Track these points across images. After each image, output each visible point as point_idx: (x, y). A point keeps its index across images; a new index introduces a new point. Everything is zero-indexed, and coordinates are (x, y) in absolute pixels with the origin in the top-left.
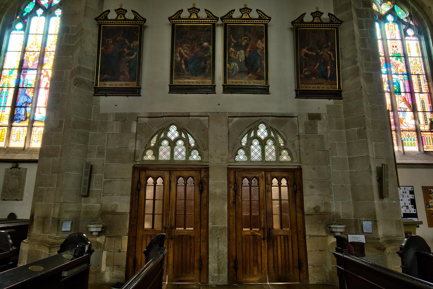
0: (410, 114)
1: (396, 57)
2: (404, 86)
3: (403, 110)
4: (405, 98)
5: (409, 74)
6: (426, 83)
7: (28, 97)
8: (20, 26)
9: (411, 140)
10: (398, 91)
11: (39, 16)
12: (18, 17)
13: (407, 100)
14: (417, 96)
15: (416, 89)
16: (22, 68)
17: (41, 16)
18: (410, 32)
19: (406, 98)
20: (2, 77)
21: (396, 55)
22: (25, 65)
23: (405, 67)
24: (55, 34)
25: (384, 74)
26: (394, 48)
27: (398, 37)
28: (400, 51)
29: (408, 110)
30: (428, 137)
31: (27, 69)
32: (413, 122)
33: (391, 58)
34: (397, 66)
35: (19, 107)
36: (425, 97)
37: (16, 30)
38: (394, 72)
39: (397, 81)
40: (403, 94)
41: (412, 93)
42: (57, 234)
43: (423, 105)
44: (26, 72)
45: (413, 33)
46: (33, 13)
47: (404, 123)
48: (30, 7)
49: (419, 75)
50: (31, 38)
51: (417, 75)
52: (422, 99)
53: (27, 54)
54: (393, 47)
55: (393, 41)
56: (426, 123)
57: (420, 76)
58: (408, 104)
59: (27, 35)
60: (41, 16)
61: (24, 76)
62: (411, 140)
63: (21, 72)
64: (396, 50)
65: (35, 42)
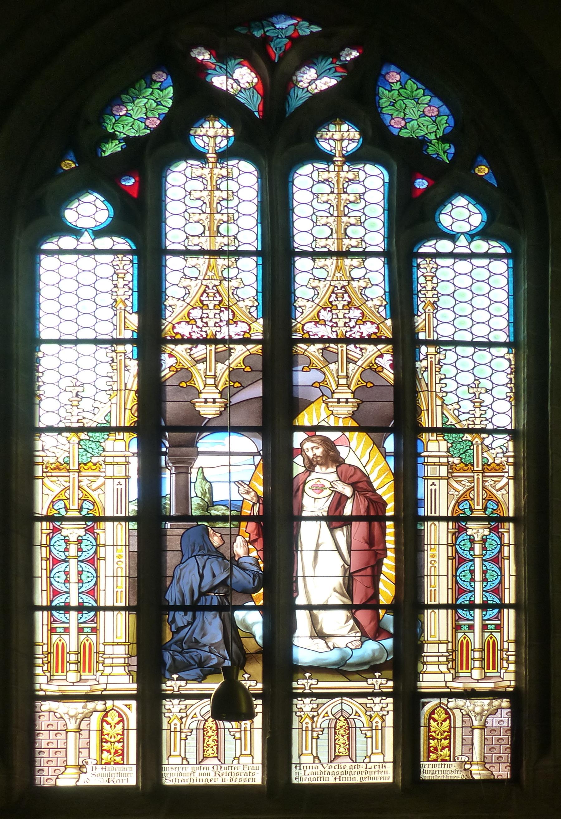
7: (234, 562)
8: (89, 210)
11: (211, 157)
12: (69, 164)
16: (161, 426)
17: (223, 156)
20: (39, 471)
22: (172, 409)
24: (127, 519)
31: (199, 427)
35: (183, 608)
42: (455, 678)
44: (193, 444)
45: (477, 219)
46: (170, 142)
50: (180, 278)
53: (172, 359)
60: (223, 156)
61: (183, 467)
63: (160, 444)
65: (212, 299)
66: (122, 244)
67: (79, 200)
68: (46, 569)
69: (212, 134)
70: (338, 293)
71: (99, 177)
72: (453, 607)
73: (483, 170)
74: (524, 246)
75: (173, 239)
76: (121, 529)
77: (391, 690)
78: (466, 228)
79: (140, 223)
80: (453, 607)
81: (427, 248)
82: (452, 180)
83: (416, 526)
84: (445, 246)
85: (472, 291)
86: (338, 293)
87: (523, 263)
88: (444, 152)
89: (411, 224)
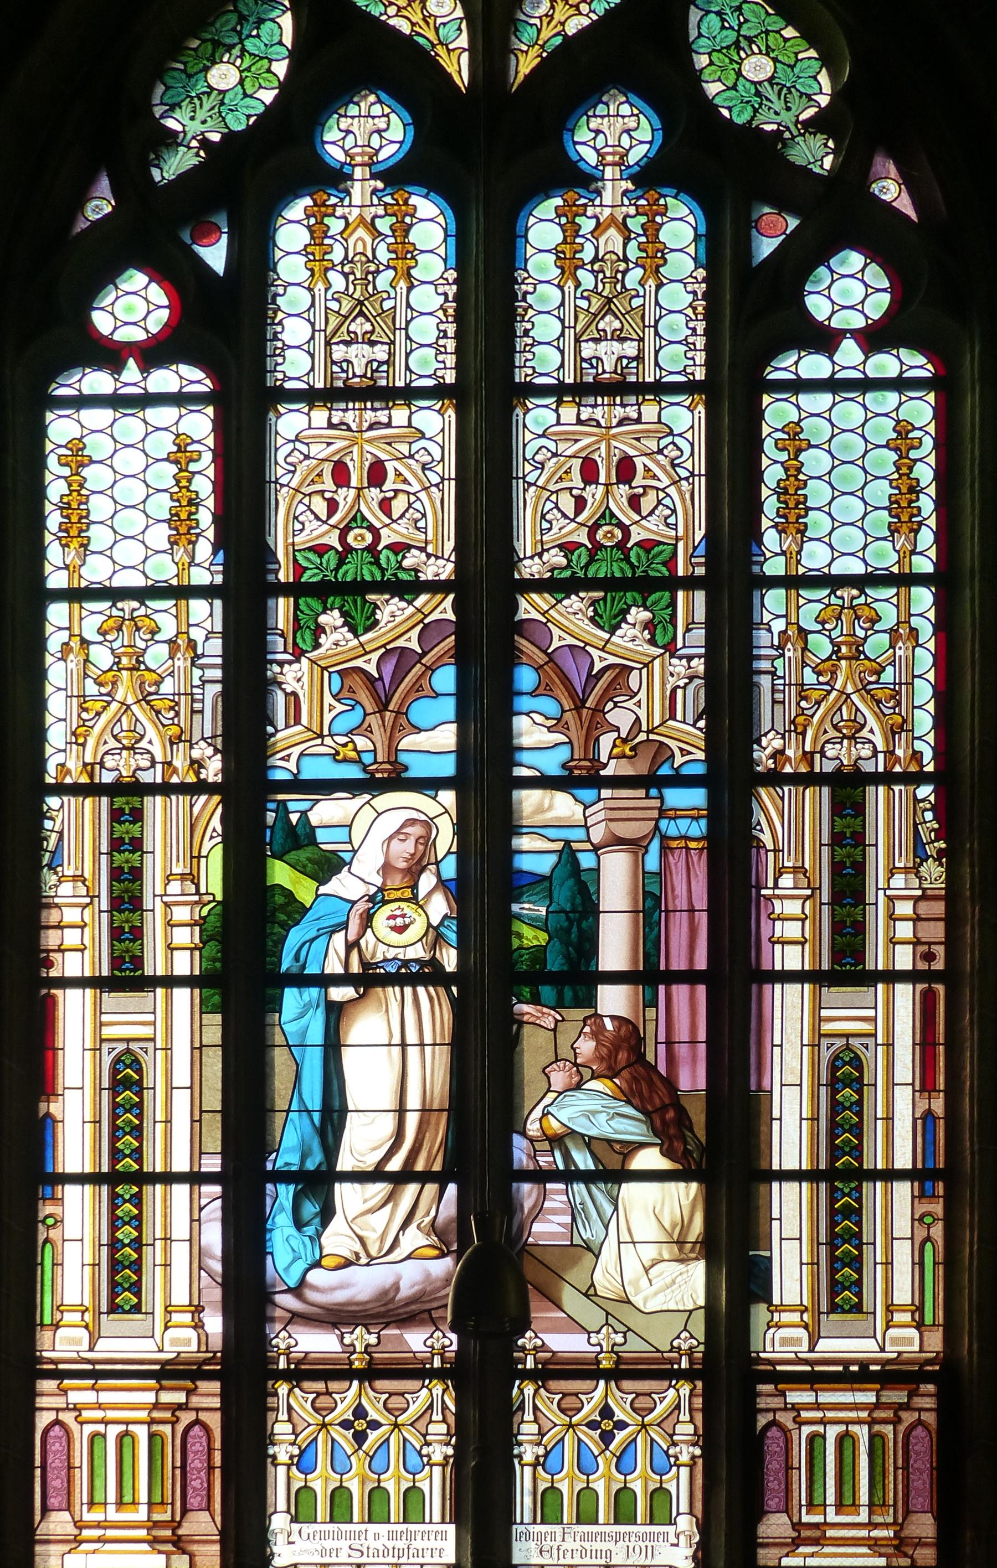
0: (658, 1206)
1: (609, 584)
2: (650, 908)
3: (583, 1161)
4: (629, 1038)
5: (733, 778)
6: (934, 871)
8: (133, 306)
9: (622, 1462)
10: (554, 964)
13: (655, 1054)
14: (788, 1009)
15: (791, 930)
18: (849, 290)
19: (653, 1032)
21: (600, 571)
23: (692, 700)
25: (544, 782)
26: (594, 494)
27: (679, 350)
28: (674, 516)
29: (650, 1159)
30: (832, 1433)
32: (690, 1284)
33: (529, 607)
34: (587, 696)
36: (894, 1020)
37: (824, 339)
38: (551, 764)
39: (568, 854)
40: (613, 1001)
41: (736, 981)
43: (835, 1107)
47: (570, 1298)
48: (232, 89)
49: (138, 789)
51: (113, 790)
52: (845, 1046)
54: (341, 474)
55: (601, 410)
56: (835, 1287)
57: (155, 806)
58: (661, 1096)
59: (245, 407)
62: (622, 1462)
64: (376, 518)
65: (371, 478)
66: (193, 378)
67: (117, 288)
68: (773, 1046)
69: (370, 130)
70: (609, 471)
71: (150, 236)
72: (112, 1179)
73: (890, 189)
74: (970, 364)
75: (294, 367)
76: (72, 966)
77: (916, 1184)
78: (858, 322)
79: (223, 329)
80: (112, 1179)
81: (785, 366)
82: (836, 217)
83: (262, 872)
84: (814, 366)
85: (855, 449)
86: (609, 471)
87: (971, 405)
88: (817, 154)
89: (755, 320)
